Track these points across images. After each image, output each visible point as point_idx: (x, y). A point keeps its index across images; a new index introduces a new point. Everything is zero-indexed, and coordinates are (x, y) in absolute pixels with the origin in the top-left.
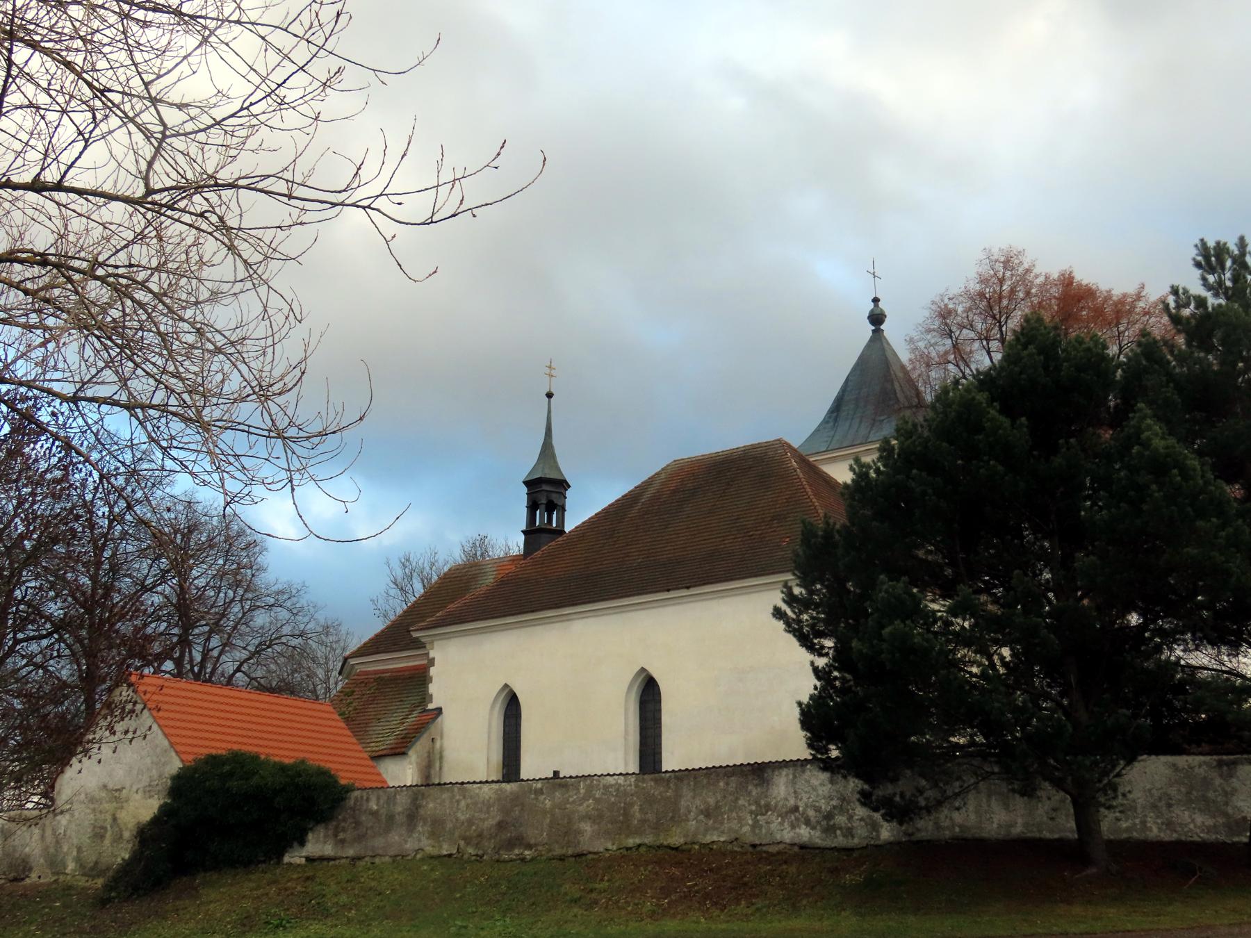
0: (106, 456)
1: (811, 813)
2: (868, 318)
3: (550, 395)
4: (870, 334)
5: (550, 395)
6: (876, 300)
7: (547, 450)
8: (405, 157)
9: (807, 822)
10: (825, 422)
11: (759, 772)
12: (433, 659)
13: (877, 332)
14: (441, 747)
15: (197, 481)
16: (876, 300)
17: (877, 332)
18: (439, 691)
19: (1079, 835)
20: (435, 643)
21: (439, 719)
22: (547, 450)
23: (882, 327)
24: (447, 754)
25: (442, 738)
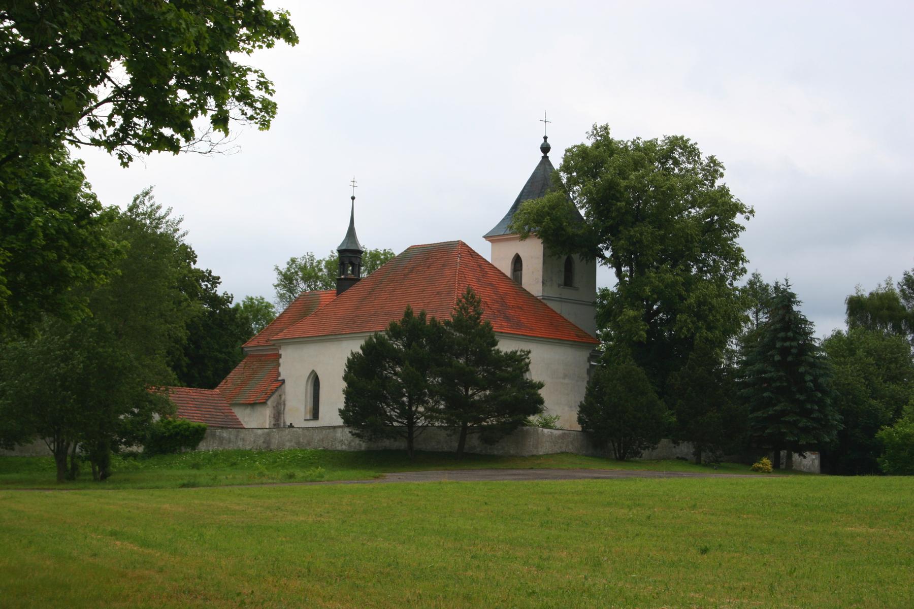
0: (115, 257)
1: (346, 442)
2: (541, 148)
3: (353, 198)
4: (541, 159)
5: (353, 198)
6: (545, 138)
7: (351, 232)
8: (220, 151)
9: (345, 444)
10: (508, 214)
11: (334, 427)
12: (281, 355)
13: (545, 158)
14: (284, 399)
15: (261, 72)
16: (545, 138)
17: (545, 158)
18: (285, 371)
19: (780, 453)
20: (282, 347)
21: (283, 386)
22: (351, 232)
23: (548, 155)
24: (287, 403)
25: (285, 394)
